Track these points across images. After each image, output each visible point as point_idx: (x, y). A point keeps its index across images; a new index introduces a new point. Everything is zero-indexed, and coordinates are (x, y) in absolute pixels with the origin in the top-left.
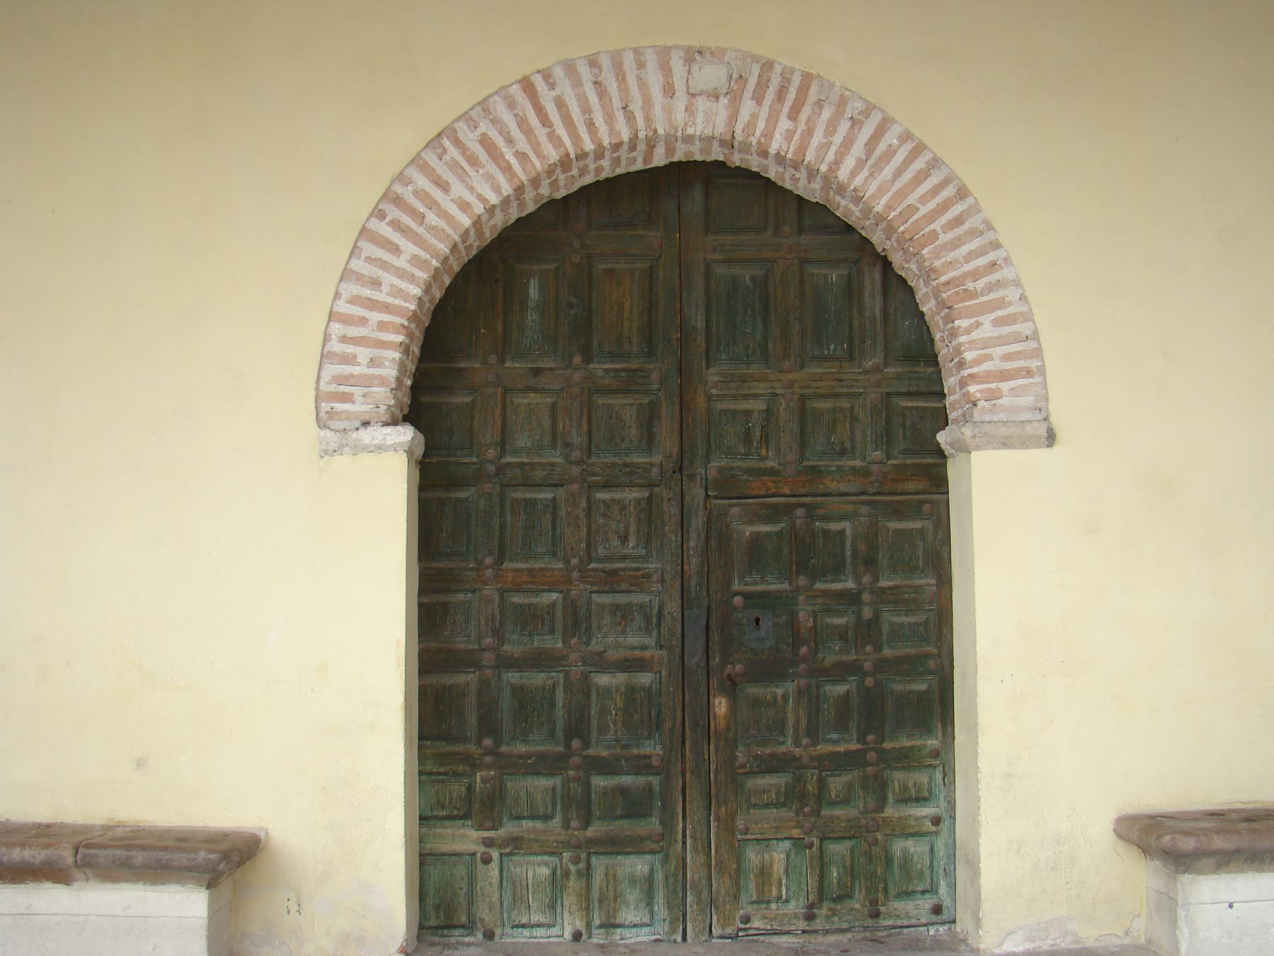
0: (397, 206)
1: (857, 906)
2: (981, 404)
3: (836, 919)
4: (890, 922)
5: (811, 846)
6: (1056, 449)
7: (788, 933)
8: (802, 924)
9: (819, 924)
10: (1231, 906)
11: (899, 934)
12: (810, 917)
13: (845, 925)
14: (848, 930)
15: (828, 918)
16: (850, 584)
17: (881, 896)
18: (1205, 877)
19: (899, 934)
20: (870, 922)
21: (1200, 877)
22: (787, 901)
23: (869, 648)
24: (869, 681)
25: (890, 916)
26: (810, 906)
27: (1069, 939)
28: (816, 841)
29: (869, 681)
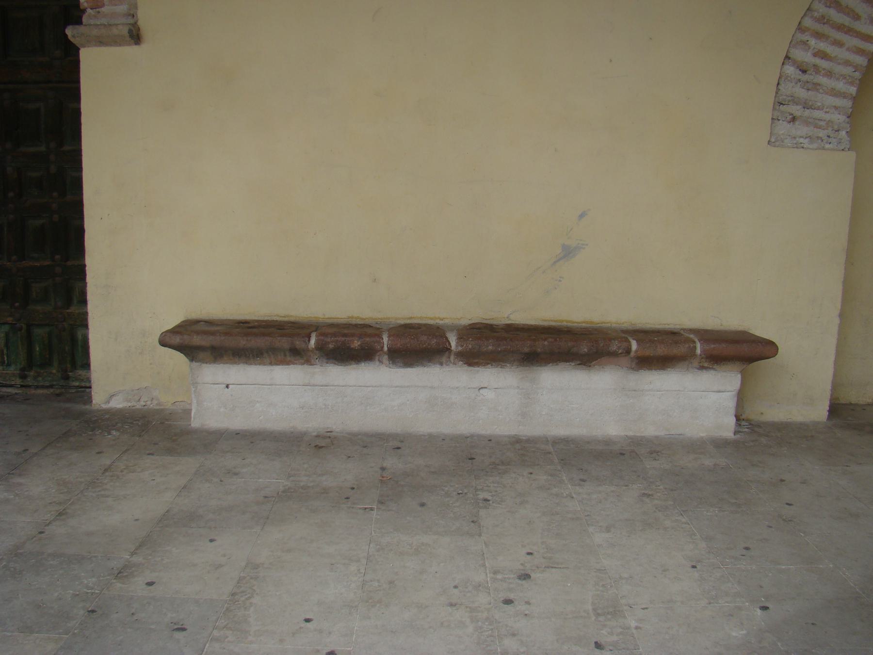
0: (827, 60)
1: (54, 371)
2: (89, 11)
3: (40, 379)
4: (77, 384)
5: (20, 329)
6: (144, 47)
7: (11, 386)
8: (19, 381)
9: (29, 381)
10: (227, 387)
11: (83, 392)
12: (23, 377)
13: (47, 384)
14: (51, 386)
15: (35, 378)
16: (43, 148)
17: (69, 366)
18: (208, 365)
19: (83, 392)
20: (62, 382)
21: (204, 365)
22: (9, 365)
23: (55, 194)
24: (56, 217)
25: (77, 379)
26: (23, 369)
27: (155, 402)
28: (24, 326)
29: (56, 217)
